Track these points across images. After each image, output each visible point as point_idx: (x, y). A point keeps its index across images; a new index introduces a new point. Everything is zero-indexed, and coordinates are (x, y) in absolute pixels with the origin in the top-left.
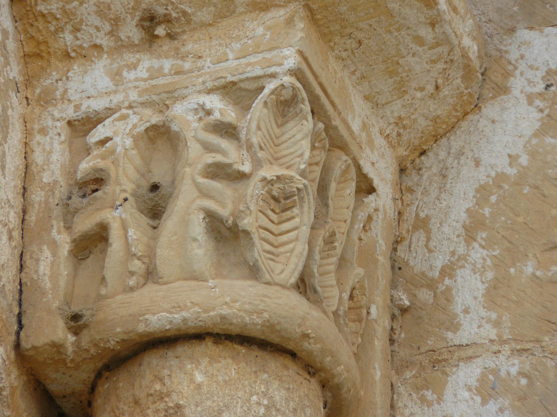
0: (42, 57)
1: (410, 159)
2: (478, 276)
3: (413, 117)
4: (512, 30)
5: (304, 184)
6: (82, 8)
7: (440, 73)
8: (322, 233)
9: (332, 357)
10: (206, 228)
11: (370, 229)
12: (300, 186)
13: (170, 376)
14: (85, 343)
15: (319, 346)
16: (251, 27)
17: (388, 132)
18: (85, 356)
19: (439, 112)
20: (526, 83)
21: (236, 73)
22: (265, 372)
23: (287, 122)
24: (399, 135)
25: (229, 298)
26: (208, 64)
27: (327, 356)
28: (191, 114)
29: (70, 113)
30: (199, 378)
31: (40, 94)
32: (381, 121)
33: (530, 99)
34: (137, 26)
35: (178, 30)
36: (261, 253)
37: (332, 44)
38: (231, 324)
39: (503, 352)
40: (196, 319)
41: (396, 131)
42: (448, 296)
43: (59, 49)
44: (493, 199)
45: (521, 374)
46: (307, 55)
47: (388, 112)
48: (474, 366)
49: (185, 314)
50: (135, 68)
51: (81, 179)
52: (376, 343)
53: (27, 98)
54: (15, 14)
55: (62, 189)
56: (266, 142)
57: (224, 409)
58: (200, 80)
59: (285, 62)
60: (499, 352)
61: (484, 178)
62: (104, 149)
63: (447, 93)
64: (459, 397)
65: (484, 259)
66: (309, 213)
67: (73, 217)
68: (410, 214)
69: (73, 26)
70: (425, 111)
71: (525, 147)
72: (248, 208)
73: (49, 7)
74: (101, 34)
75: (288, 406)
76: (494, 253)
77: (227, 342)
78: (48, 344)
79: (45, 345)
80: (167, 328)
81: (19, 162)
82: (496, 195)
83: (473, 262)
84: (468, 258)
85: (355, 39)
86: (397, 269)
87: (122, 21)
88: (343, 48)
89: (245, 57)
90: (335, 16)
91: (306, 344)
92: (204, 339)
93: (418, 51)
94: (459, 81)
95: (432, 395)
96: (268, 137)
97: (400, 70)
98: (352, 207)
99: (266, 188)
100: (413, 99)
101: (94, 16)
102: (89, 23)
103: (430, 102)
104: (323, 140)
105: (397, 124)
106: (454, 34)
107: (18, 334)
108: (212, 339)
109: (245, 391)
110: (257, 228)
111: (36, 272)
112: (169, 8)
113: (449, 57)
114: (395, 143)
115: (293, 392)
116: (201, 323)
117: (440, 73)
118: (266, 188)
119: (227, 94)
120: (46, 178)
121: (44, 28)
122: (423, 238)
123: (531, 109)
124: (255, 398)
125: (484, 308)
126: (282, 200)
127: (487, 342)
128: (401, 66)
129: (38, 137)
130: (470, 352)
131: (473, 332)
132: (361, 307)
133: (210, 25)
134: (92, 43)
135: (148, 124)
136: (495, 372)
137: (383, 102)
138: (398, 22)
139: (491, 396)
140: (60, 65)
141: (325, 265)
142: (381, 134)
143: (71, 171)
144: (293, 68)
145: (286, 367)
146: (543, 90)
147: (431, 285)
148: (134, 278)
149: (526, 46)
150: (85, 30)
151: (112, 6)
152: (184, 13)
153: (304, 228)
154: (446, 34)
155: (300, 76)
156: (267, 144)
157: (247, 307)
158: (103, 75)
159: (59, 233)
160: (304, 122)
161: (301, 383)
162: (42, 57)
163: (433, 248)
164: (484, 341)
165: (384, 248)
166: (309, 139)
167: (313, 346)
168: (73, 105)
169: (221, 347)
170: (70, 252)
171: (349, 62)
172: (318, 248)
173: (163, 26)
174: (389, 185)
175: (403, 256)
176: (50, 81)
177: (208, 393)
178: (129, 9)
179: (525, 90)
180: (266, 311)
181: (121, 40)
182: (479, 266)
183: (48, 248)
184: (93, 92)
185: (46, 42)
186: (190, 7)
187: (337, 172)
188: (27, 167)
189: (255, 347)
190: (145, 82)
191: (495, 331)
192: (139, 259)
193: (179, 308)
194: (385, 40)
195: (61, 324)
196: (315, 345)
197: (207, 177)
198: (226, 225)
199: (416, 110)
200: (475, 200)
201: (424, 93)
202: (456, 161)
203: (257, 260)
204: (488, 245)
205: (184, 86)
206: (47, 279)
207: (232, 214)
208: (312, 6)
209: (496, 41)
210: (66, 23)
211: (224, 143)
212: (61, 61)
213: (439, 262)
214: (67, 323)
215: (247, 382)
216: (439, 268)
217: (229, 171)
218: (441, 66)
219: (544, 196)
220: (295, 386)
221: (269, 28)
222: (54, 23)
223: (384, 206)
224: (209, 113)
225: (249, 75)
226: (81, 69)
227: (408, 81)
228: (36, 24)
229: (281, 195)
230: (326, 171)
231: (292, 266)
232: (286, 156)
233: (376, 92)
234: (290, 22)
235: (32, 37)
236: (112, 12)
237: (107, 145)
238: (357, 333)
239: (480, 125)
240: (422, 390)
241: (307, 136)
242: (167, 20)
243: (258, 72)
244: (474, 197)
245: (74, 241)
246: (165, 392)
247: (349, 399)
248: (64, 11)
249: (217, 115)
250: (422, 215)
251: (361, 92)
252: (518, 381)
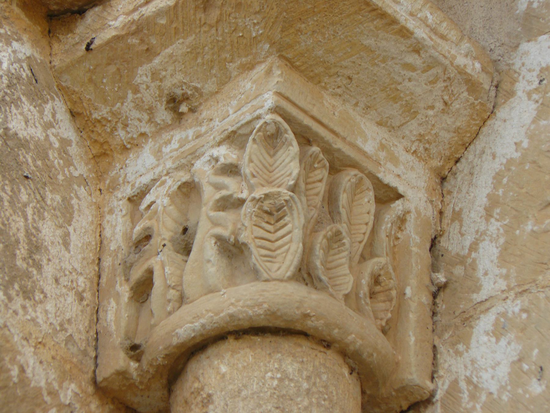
0: (107, 155)
1: (447, 168)
2: (494, 244)
3: (433, 132)
4: (517, 46)
5: (290, 196)
6: (124, 107)
7: (443, 91)
9: (339, 329)
10: (219, 250)
11: (405, 228)
12: (287, 198)
13: (202, 374)
14: (145, 367)
15: (322, 322)
16: (243, 85)
17: (413, 149)
18: (148, 377)
19: (458, 124)
20: (526, 83)
21: (234, 123)
22: (278, 352)
23: (277, 151)
24: (426, 149)
25: (234, 299)
26: (217, 123)
27: (334, 329)
28: (207, 165)
29: (128, 191)
30: (224, 369)
31: (109, 185)
32: (403, 140)
33: (529, 95)
34: (166, 109)
35: (196, 104)
36: (258, 258)
37: (323, 84)
38: (239, 320)
39: (510, 298)
40: (211, 323)
41: (422, 146)
42: (474, 267)
43: (118, 145)
44: (505, 180)
45: (523, 310)
46: (288, 94)
47: (407, 133)
48: (490, 314)
49: (203, 321)
50: (170, 143)
51: (135, 240)
52: (411, 316)
53: (100, 190)
54: (78, 126)
55: (123, 252)
56: (258, 170)
57: (243, 388)
58: (212, 137)
59: (266, 104)
60: (507, 298)
61: (499, 166)
62: (150, 211)
63: (458, 106)
64: (480, 342)
65: (498, 229)
66: (299, 218)
67: (130, 270)
69: (122, 124)
70: (443, 125)
71: (526, 133)
72: (243, 225)
73: (100, 114)
74: (143, 124)
75: (302, 375)
76: (505, 223)
77: (245, 336)
78: (114, 374)
79: (112, 375)
80: (193, 335)
81: (92, 239)
82: (507, 177)
83: (491, 234)
84: (487, 232)
85: (343, 76)
86: (441, 257)
87: (155, 109)
88: (335, 85)
89: (239, 109)
90: (314, 60)
91: (309, 323)
92: (227, 338)
93: (412, 76)
94: (466, 94)
95: (463, 347)
96: (261, 166)
97: (402, 95)
98: (373, 211)
99: (257, 206)
100: (426, 117)
101: (134, 111)
102: (132, 118)
103: (445, 117)
104: (321, 161)
105: (420, 141)
106: (441, 56)
107: (94, 372)
108: (233, 337)
109: (261, 371)
110: (253, 239)
111: (106, 320)
112: (184, 88)
113: (446, 76)
114: (425, 157)
115: (307, 364)
116: (216, 325)
117: (443, 91)
118: (257, 206)
119: (232, 142)
121: (102, 131)
122: (458, 227)
123: (530, 102)
124: (269, 374)
125: (498, 267)
126: (275, 213)
127: (499, 293)
128: (401, 92)
129: (108, 217)
130: (487, 305)
131: (490, 289)
132: (390, 289)
133: (217, 92)
134: (139, 133)
135: (179, 183)
136: (504, 315)
137: (398, 124)
138: (381, 55)
139: (502, 334)
140: (121, 157)
141: (337, 260)
142: (407, 151)
143: (127, 236)
144: (272, 107)
145: (300, 346)
146: (538, 86)
148: (171, 304)
149: (525, 55)
150: (131, 124)
151: (144, 99)
152: (196, 89)
153: (296, 231)
154: (433, 57)
155: (281, 113)
156: (260, 172)
157: (249, 303)
158: (149, 155)
159: (121, 285)
160: (291, 148)
161: (316, 356)
162: (107, 155)
163: (464, 232)
164: (497, 293)
165: (418, 241)
166: (297, 160)
167: (316, 322)
168: (130, 185)
169: (241, 341)
170: (131, 298)
171: (347, 97)
173: (185, 104)
174: (423, 191)
175: (444, 245)
176: (115, 172)
177: (230, 379)
178: (156, 97)
179: (526, 90)
180: (265, 302)
181: (159, 124)
182: (494, 236)
183: (114, 300)
184: (143, 170)
185: (107, 142)
186: (199, 83)
188: (101, 243)
189: (269, 335)
190: (177, 151)
191: (505, 283)
192: (173, 288)
193: (198, 317)
194: (375, 72)
195: (122, 355)
196: (318, 321)
197: (219, 211)
198: (230, 242)
199: (433, 125)
200: (492, 185)
201: (435, 110)
202: (480, 160)
203: (255, 265)
205: (201, 145)
206: (113, 324)
207: (233, 233)
208: (287, 56)
209: (506, 59)
210: (116, 122)
211: (227, 180)
212: (121, 154)
213: (468, 241)
214: (128, 354)
215: (262, 364)
216: (468, 246)
217: (232, 201)
218: (441, 84)
219: (540, 167)
220: (309, 358)
221: (254, 82)
222: (108, 125)
223: (416, 208)
224: (217, 160)
225: (243, 122)
226: (135, 156)
227: (414, 103)
228: (95, 129)
229: (273, 209)
231: (287, 262)
232: (278, 178)
233: (387, 117)
234: (269, 72)
235: (96, 141)
236: (146, 103)
237: (152, 208)
238: (387, 310)
239: (496, 127)
240: (456, 345)
241: (295, 158)
242: (186, 98)
243: (248, 118)
244: (492, 183)
245: (132, 289)
246: (200, 387)
247: (376, 362)
248: (113, 114)
249: (222, 160)
250: (457, 209)
251: (372, 120)
252: (521, 317)
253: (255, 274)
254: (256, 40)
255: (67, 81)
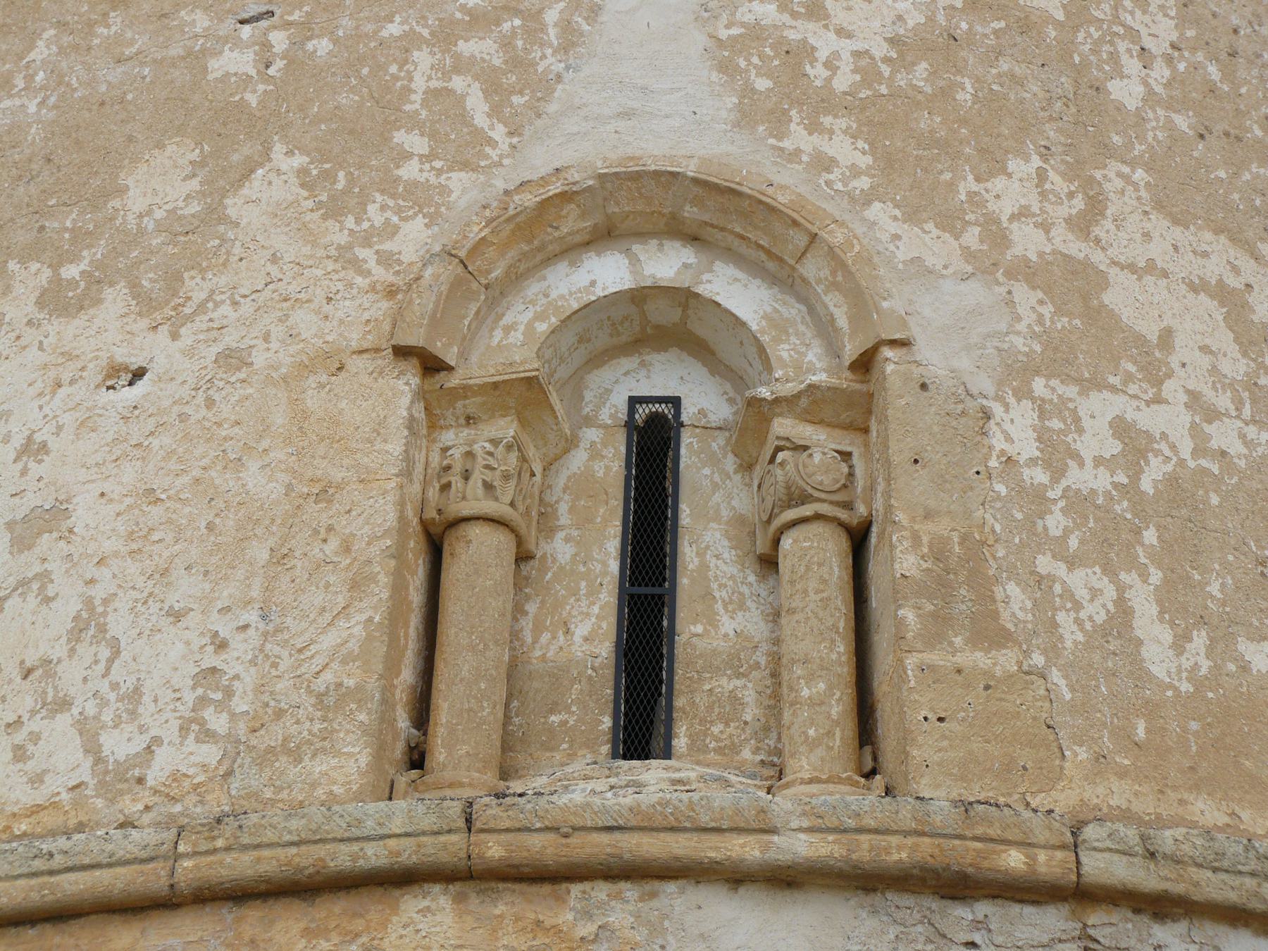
8: (519, 488)
29: (442, 446)
68: (546, 483)
120: (433, 466)
143: (440, 464)
147: (552, 506)
172: (407, 662)
187: (524, 469)
204: (569, 495)
211: (490, 458)
213: (554, 499)
230: (521, 468)
234: (512, 421)
242: (474, 418)
253: (496, 499)
254: (510, 408)
255: (427, 396)
